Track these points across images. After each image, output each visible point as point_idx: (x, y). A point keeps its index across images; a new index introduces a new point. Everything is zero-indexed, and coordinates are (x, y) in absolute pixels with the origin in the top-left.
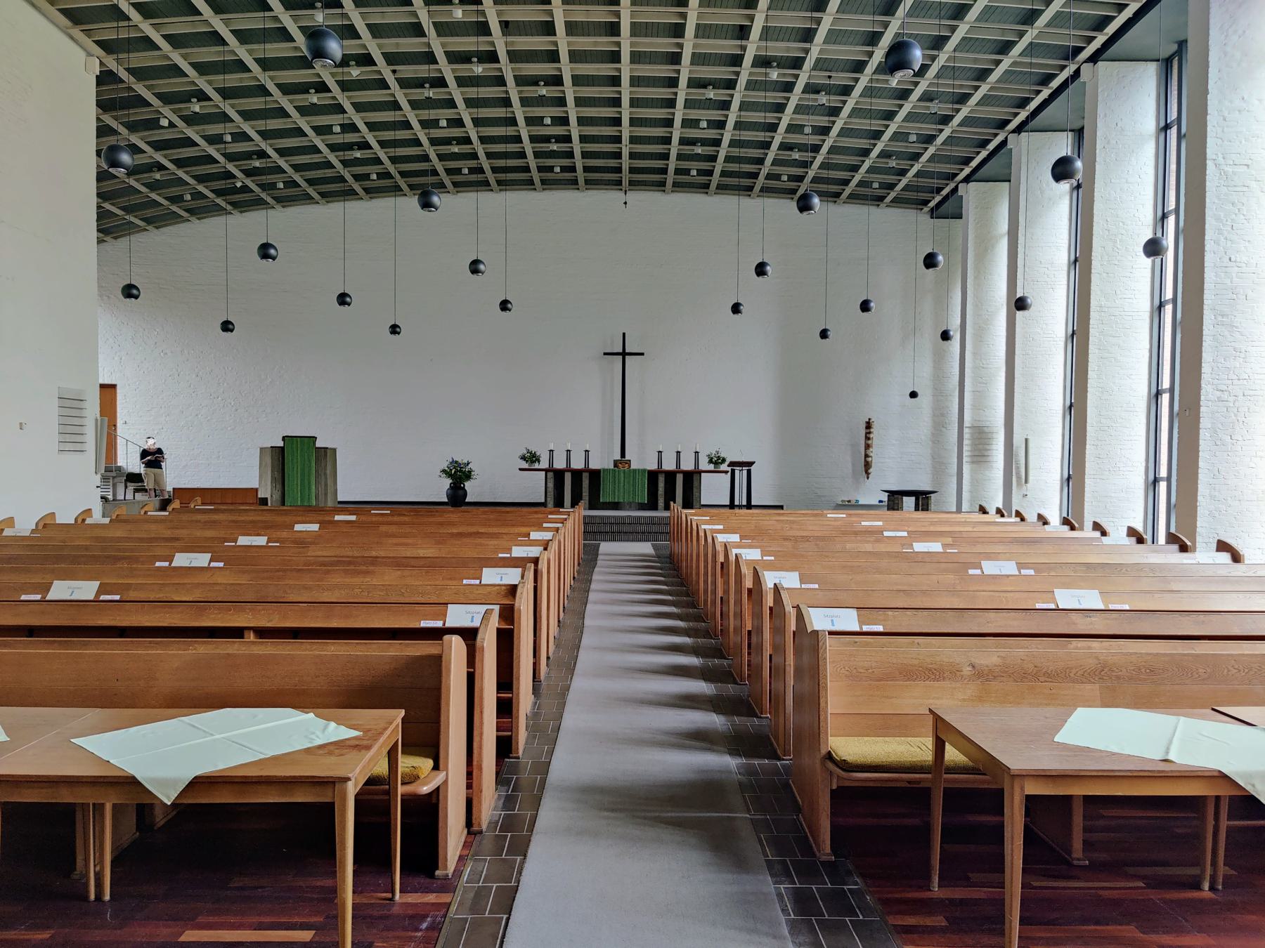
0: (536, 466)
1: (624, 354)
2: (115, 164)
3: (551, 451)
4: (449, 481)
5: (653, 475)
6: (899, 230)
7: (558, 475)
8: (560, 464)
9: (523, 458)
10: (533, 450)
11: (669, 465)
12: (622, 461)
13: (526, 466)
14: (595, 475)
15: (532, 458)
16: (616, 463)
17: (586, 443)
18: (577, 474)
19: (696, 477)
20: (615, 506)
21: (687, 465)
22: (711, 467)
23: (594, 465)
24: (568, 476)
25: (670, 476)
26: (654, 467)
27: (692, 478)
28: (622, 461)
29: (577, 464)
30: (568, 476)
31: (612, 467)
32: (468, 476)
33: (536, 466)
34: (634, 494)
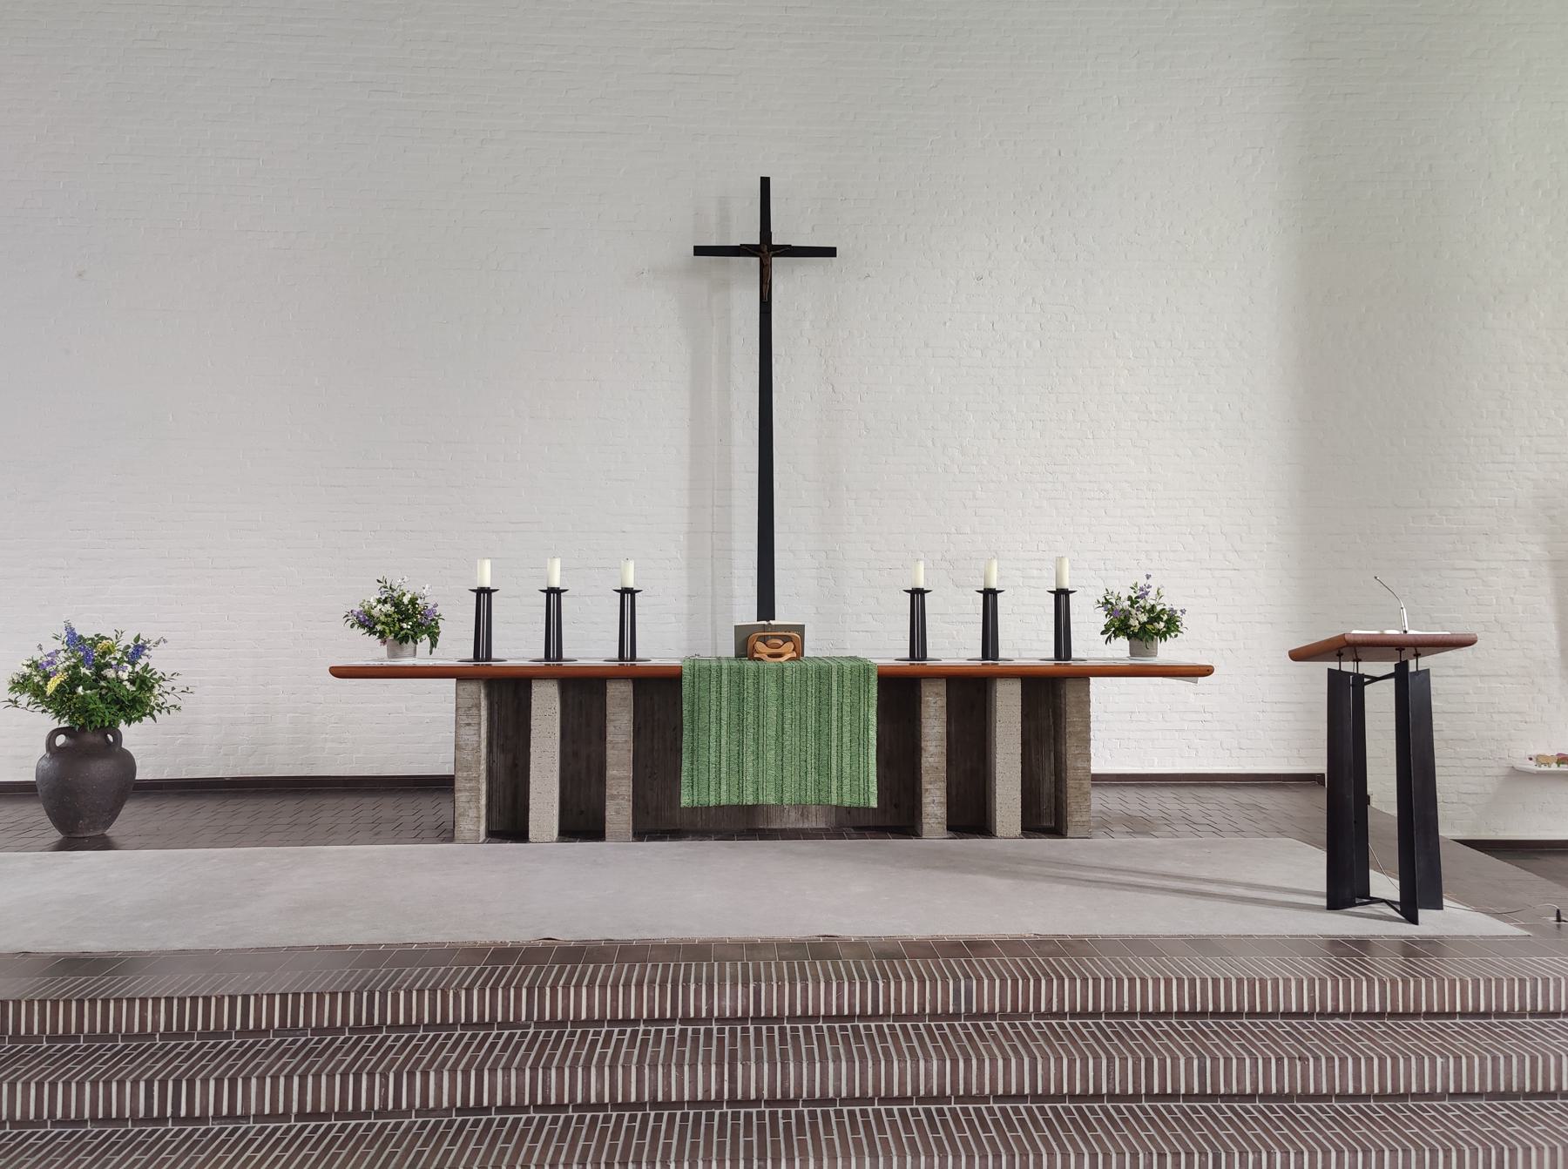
0: (421, 654)
1: (765, 251)
2: (721, 960)
3: (484, 594)
4: (48, 722)
5: (899, 691)
6: (56, 835)
7: (505, 693)
8: (518, 646)
9: (367, 622)
10: (409, 586)
11: (954, 645)
12: (765, 636)
13: (372, 651)
14: (659, 692)
15: (403, 621)
16: (745, 643)
17: (616, 550)
18: (583, 690)
19: (1070, 693)
20: (743, 824)
21: (1027, 642)
22: (1119, 650)
23: (659, 647)
24: (546, 706)
25: (970, 691)
26: (891, 650)
27: (1053, 694)
28: (765, 636)
29: (589, 645)
30: (546, 706)
31: (728, 649)
32: (136, 700)
33: (421, 654)
34: (823, 768)
